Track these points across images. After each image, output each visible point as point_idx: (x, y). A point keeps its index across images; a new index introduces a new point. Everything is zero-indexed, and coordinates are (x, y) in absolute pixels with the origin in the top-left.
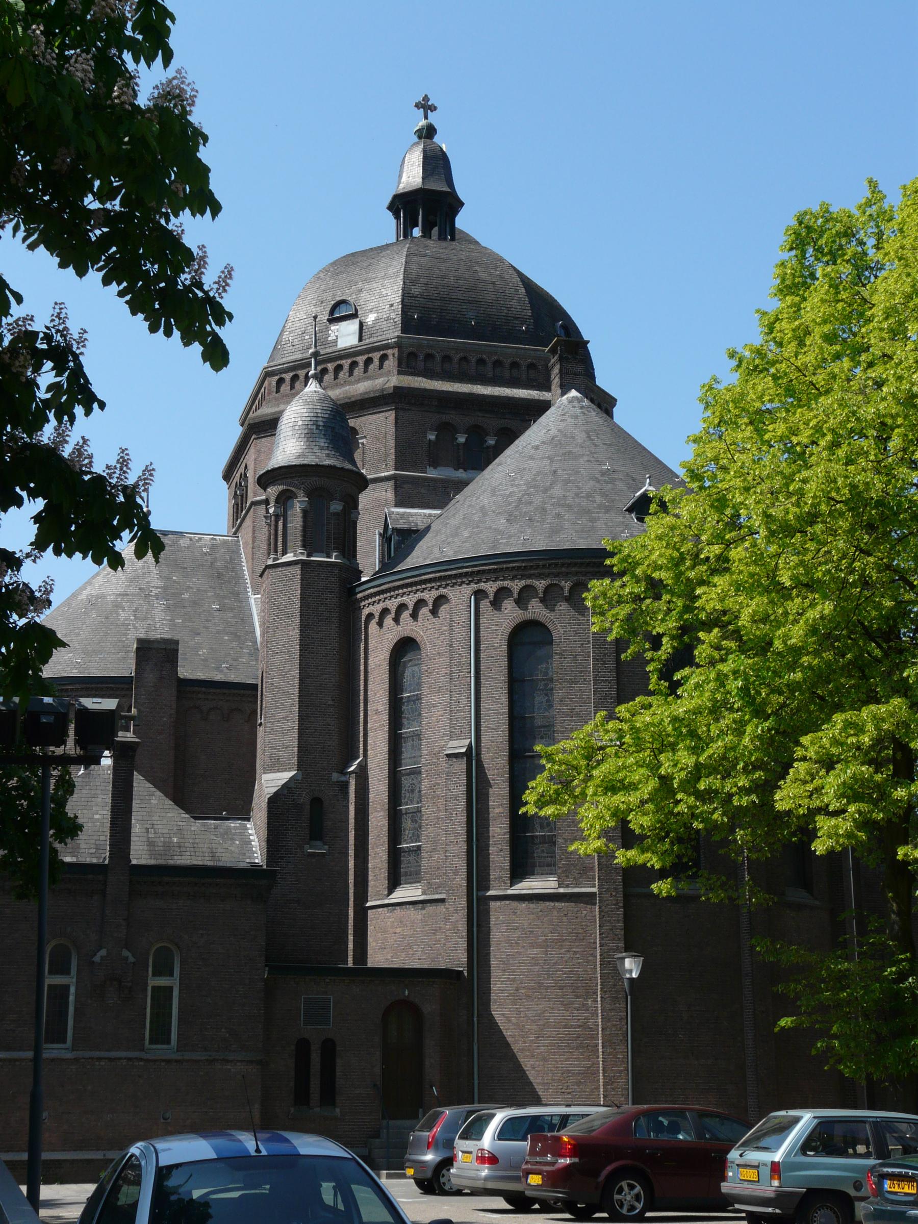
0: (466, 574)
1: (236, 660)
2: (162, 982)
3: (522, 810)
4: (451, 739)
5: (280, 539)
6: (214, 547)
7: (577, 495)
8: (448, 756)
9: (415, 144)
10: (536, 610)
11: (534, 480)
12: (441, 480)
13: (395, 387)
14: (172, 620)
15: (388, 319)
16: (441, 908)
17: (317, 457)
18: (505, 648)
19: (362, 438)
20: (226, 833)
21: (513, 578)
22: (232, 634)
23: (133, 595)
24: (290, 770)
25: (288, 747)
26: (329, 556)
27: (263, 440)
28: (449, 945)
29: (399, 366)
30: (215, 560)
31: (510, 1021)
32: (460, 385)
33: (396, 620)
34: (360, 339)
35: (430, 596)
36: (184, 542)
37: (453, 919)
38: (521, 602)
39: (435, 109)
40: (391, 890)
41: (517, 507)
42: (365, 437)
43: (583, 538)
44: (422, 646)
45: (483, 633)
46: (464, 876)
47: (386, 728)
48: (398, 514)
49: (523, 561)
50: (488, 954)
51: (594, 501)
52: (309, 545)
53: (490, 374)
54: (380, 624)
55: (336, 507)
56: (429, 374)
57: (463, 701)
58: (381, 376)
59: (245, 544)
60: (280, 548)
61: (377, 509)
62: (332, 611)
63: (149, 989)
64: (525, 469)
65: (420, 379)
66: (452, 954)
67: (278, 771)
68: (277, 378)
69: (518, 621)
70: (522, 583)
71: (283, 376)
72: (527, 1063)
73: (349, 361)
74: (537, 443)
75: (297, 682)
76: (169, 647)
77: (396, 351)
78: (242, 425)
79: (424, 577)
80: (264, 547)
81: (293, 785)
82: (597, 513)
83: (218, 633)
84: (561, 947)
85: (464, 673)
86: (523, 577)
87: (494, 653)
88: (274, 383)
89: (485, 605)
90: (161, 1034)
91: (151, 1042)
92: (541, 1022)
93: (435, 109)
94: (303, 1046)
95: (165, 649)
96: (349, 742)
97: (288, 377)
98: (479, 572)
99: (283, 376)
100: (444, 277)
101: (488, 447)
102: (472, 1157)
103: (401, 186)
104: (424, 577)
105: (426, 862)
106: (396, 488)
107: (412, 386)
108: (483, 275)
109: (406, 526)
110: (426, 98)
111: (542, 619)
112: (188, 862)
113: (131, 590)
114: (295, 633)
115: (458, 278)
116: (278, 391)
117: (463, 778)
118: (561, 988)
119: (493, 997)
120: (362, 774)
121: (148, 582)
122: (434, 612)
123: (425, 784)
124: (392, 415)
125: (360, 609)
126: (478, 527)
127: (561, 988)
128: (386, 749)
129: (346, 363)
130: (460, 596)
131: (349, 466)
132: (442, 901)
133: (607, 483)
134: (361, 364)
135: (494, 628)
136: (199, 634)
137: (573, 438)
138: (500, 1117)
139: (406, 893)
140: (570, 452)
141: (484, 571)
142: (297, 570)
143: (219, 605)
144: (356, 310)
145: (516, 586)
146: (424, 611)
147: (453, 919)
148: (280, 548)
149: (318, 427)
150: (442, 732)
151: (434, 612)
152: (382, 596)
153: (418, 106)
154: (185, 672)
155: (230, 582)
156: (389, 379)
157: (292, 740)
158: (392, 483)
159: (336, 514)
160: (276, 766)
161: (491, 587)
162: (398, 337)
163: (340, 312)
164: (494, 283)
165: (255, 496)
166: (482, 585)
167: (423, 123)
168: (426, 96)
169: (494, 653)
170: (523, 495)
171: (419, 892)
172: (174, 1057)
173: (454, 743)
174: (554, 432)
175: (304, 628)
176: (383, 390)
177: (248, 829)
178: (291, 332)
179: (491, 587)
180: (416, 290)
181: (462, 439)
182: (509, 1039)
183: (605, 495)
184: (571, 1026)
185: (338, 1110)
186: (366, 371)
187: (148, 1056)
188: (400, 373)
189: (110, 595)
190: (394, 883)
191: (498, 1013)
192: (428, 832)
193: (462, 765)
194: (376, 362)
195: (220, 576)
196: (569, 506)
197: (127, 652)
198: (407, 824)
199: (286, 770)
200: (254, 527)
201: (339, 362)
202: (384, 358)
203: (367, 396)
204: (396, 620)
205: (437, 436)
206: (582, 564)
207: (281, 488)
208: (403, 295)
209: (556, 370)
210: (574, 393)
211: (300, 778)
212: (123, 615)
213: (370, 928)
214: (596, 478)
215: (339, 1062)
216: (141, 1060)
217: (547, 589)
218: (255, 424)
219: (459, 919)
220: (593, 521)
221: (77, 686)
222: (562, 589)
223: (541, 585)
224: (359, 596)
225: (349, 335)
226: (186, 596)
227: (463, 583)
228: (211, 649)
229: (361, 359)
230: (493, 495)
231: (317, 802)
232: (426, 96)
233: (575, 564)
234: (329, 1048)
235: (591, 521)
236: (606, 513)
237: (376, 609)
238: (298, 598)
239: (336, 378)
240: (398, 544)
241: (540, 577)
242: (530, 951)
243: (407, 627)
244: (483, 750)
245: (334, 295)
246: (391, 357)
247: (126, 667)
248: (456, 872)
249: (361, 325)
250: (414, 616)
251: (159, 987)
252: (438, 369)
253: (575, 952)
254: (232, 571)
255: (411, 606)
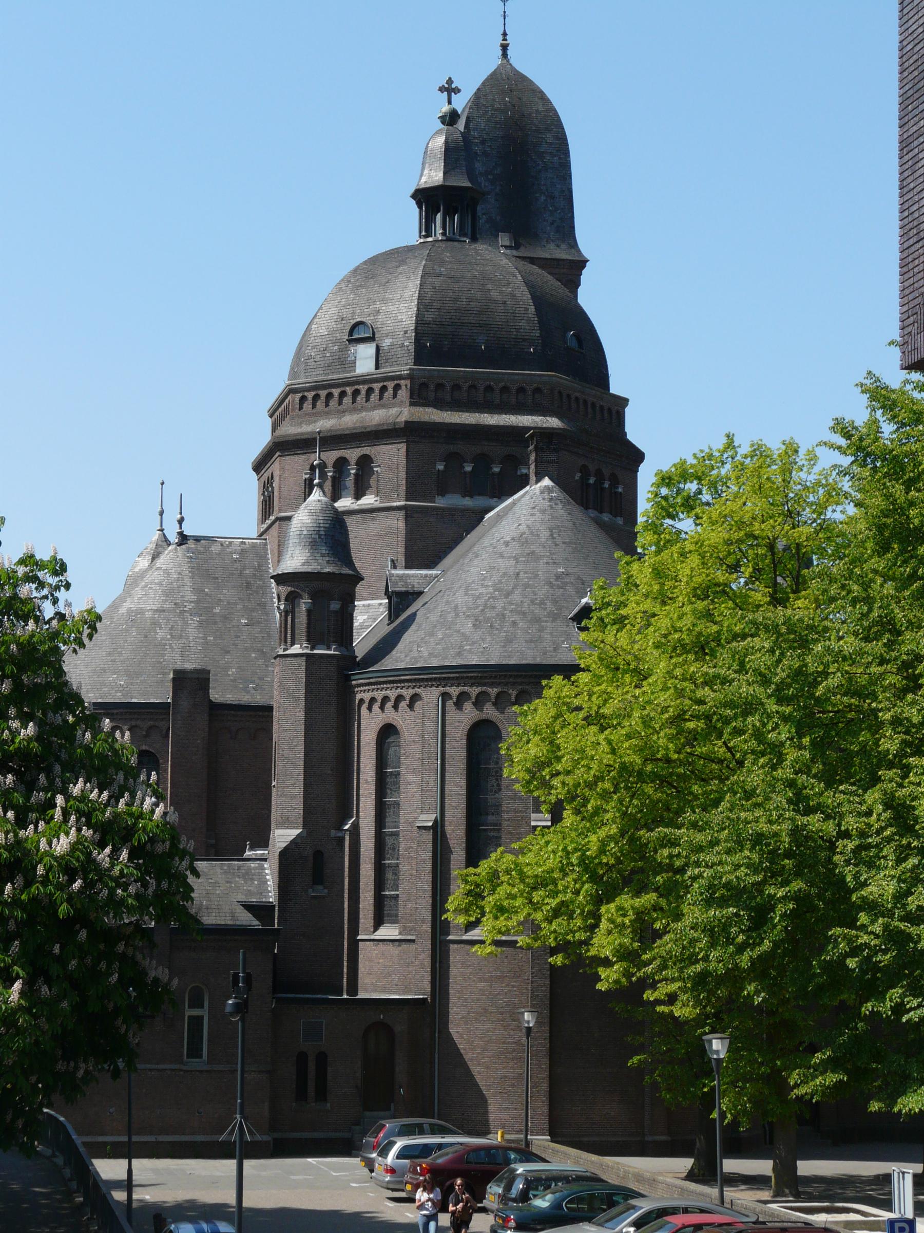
0: (435, 679)
1: (261, 679)
2: (196, 1012)
3: (445, 916)
4: (422, 813)
5: (289, 632)
6: (243, 552)
7: (532, 601)
8: (419, 827)
9: (438, 132)
10: (489, 711)
11: (500, 582)
12: (449, 509)
13: (406, 422)
14: (205, 638)
15: (402, 346)
16: (413, 947)
17: (319, 564)
18: (464, 741)
19: (376, 467)
20: (247, 874)
21: (472, 685)
22: (258, 650)
23: (169, 611)
24: (297, 828)
25: (295, 808)
26: (329, 648)
27: (287, 458)
28: (417, 977)
29: (411, 397)
30: (244, 568)
31: (462, 1037)
32: (467, 414)
33: (382, 708)
34: (377, 367)
35: (407, 693)
36: (216, 548)
37: (421, 957)
38: (479, 703)
39: (459, 91)
40: (376, 928)
41: (483, 610)
42: (379, 466)
43: (529, 649)
44: (401, 733)
45: (448, 728)
46: (430, 924)
47: (374, 797)
48: (398, 576)
49: (479, 672)
50: (448, 985)
51: (545, 609)
52: (313, 641)
53: (497, 401)
54: (370, 709)
55: (335, 606)
56: (440, 404)
57: (432, 783)
58: (394, 406)
59: (272, 551)
60: (289, 640)
61: (368, 616)
62: (336, 682)
63: (186, 1018)
64: (494, 567)
65: (430, 410)
66: (418, 987)
67: (288, 828)
68: (300, 395)
69: (475, 719)
70: (479, 689)
71: (306, 394)
72: (475, 1069)
73: (366, 387)
74: (508, 539)
75: (302, 755)
76: (201, 676)
77: (408, 382)
78: (271, 416)
79: (403, 678)
80: (278, 641)
81: (299, 841)
82: (546, 621)
83: (246, 650)
84: (502, 982)
85: (432, 760)
86: (480, 684)
87: (455, 745)
88: (297, 400)
89: (450, 704)
90: (194, 1051)
91: (188, 1057)
92: (486, 1039)
93: (459, 91)
94: (302, 1058)
95: (198, 678)
96: (345, 805)
97: (310, 395)
98: (445, 678)
99: (306, 394)
100: (456, 300)
101: (493, 474)
102: (382, 1168)
103: (424, 179)
104: (403, 678)
105: (403, 908)
106: (407, 518)
107: (422, 420)
108: (495, 294)
109: (404, 589)
110: (450, 81)
111: (493, 719)
112: (214, 922)
113: (168, 606)
114: (301, 715)
115: (470, 300)
116: (301, 408)
117: (430, 847)
118: (502, 1013)
119: (451, 1018)
120: (356, 827)
121: (183, 596)
122: (411, 706)
123: (402, 846)
124: (403, 447)
125: (354, 694)
126: (450, 628)
127: (502, 1013)
128: (373, 813)
129: (363, 388)
130: (431, 695)
131: (346, 571)
132: (413, 941)
133: (559, 587)
134: (377, 391)
135: (457, 724)
136: (228, 652)
137: (538, 535)
138: (400, 1144)
139: (388, 931)
140: (533, 553)
141: (449, 678)
142: (302, 662)
143: (247, 619)
144: (374, 333)
145: (474, 691)
146: (403, 705)
147: (421, 957)
148: (289, 640)
149: (320, 536)
150: (416, 809)
151: (411, 706)
152: (370, 687)
153: (442, 89)
154: (216, 695)
155: (257, 592)
156: (400, 411)
157: (298, 803)
158: (402, 513)
159: (336, 612)
160: (286, 824)
161: (454, 691)
162: (410, 369)
163: (359, 333)
164: (505, 303)
165: (280, 511)
166: (448, 689)
167: (446, 108)
168: (450, 78)
169: (455, 745)
170: (489, 598)
171: (397, 932)
172: (205, 1068)
173: (423, 817)
174: (523, 528)
175: (308, 710)
176: (395, 424)
177: (265, 869)
178: (313, 348)
179: (454, 691)
180: (429, 317)
181: (468, 468)
182: (462, 1051)
183: (555, 602)
184: (508, 1043)
185: (329, 1105)
186: (381, 398)
187: (185, 1068)
188: (412, 404)
189: (148, 611)
190: (378, 922)
191: (454, 1031)
192: (404, 885)
193: (429, 836)
194: (390, 391)
195: (248, 586)
196: (524, 614)
197: (164, 674)
198: (389, 875)
199: (293, 828)
200: (279, 541)
201: (356, 387)
202: (397, 388)
203: (380, 428)
204: (382, 708)
205: (445, 466)
206: (526, 676)
207: (290, 589)
208: (417, 323)
209: (533, 457)
210: (546, 482)
211: (305, 834)
212: (160, 634)
213: (361, 957)
214: (551, 583)
215: (329, 1069)
216: (181, 1070)
217: (498, 695)
218: (279, 443)
219: (425, 958)
220: (541, 630)
221: (121, 710)
222: (510, 695)
223: (493, 691)
224: (354, 683)
225: (366, 358)
226: (217, 610)
227: (432, 685)
228: (239, 668)
229: (377, 386)
230: (466, 594)
231: (318, 855)
232: (450, 78)
233: (521, 676)
234: (322, 1060)
235: (539, 631)
236: (553, 621)
237: (367, 696)
238: (303, 685)
239: (354, 401)
240: (398, 604)
241: (492, 685)
242: (479, 984)
243: (389, 715)
244: (447, 823)
245: (353, 313)
246: (403, 387)
247: (163, 694)
248: (423, 921)
249: (378, 349)
250: (396, 707)
251: (194, 1016)
252: (448, 398)
253: (513, 986)
254: (260, 580)
255: (393, 698)
